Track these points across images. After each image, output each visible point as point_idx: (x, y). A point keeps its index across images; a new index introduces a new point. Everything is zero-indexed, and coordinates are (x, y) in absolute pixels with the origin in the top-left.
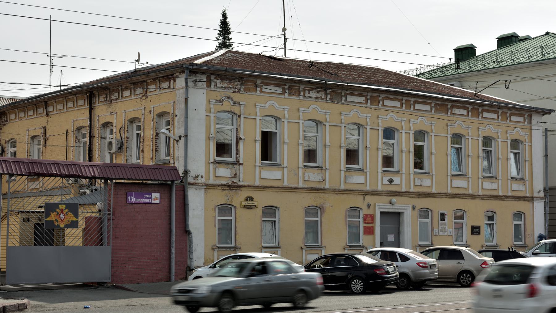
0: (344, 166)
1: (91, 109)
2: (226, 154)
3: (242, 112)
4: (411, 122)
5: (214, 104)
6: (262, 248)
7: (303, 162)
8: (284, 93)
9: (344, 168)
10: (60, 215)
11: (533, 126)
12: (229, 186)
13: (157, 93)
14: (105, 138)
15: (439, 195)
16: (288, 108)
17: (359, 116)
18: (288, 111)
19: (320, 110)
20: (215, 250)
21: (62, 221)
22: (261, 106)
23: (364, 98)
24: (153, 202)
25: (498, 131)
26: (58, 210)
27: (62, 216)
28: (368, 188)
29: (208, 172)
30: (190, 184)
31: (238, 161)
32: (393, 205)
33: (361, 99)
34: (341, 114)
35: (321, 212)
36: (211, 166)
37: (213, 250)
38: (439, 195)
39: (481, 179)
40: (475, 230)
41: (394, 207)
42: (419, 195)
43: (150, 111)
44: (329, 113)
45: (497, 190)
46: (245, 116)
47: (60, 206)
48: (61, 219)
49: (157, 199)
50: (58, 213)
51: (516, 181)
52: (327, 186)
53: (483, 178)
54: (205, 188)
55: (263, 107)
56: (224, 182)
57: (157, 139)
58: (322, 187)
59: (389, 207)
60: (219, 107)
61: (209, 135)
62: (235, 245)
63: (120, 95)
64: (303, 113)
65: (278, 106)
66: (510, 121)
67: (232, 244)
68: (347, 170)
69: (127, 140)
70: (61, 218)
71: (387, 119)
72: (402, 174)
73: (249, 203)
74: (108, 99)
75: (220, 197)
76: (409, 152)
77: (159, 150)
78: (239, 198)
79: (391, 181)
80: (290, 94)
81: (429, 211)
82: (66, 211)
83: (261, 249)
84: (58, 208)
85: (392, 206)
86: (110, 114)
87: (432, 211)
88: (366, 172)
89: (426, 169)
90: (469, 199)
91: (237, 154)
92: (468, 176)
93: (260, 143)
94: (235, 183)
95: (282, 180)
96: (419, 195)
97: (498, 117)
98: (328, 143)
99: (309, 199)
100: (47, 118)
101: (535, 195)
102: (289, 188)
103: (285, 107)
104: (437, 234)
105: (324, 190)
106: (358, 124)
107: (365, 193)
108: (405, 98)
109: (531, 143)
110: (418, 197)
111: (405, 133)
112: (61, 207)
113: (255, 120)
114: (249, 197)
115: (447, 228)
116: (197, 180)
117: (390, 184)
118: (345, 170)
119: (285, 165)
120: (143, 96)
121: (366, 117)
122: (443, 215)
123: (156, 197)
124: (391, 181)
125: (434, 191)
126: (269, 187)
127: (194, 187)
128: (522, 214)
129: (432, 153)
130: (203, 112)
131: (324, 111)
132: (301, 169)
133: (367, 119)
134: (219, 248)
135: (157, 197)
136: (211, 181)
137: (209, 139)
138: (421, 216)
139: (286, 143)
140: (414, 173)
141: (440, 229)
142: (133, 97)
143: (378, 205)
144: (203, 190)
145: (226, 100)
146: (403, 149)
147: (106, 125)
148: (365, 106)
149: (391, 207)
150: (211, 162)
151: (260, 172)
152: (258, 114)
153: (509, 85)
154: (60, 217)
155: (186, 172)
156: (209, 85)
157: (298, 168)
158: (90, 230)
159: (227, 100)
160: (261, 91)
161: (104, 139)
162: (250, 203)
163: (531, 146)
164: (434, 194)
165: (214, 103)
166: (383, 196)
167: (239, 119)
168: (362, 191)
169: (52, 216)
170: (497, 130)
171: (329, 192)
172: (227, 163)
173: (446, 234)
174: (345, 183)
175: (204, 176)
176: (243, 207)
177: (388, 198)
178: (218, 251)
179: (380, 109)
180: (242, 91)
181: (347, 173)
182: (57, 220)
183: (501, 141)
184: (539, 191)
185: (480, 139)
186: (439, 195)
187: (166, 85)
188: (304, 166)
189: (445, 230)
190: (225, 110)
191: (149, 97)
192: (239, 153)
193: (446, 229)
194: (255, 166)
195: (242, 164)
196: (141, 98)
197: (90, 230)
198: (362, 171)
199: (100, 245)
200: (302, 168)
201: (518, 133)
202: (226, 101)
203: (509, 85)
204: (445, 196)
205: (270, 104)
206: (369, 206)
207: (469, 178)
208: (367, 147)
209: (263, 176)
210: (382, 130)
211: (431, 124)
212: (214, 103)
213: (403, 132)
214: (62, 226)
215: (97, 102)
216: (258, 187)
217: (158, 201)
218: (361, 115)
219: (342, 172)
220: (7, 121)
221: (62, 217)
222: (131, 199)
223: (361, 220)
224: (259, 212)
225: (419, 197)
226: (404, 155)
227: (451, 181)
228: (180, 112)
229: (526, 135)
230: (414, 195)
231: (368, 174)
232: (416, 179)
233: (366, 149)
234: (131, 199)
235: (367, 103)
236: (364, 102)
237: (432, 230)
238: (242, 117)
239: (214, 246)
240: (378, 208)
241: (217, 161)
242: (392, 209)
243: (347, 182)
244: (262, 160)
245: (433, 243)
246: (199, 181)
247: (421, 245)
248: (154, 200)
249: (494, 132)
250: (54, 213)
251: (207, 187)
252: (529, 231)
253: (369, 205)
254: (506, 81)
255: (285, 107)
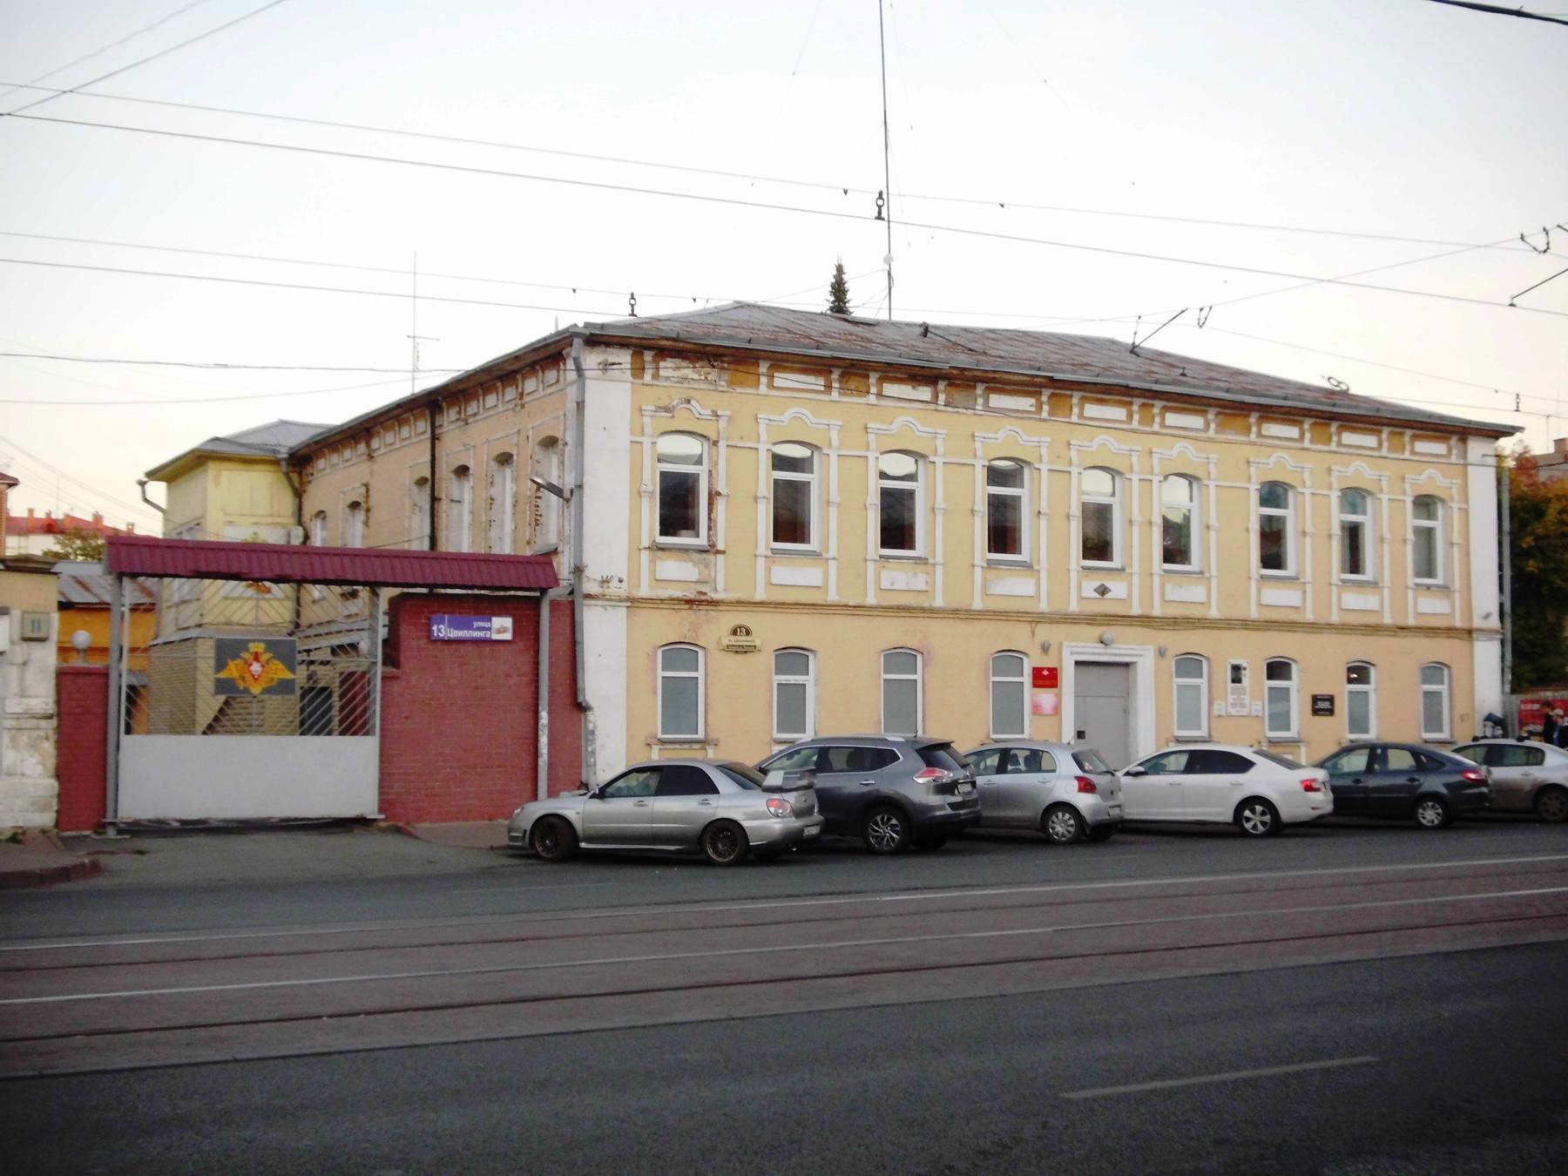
0: (767, 543)
1: (434, 438)
2: (687, 529)
3: (722, 435)
4: (1154, 455)
5: (652, 417)
6: (773, 743)
7: (1162, 561)
8: (829, 387)
9: (766, 550)
10: (251, 665)
11: (590, 379)
12: (690, 602)
13: (538, 396)
14: (459, 502)
15: (1229, 624)
16: (1049, 440)
17: (1021, 442)
18: (839, 431)
19: (920, 428)
20: (653, 746)
21: (256, 680)
22: (770, 420)
23: (1032, 401)
24: (495, 637)
25: (1208, 458)
26: (246, 655)
27: (256, 667)
28: (1043, 606)
29: (634, 569)
30: (589, 596)
31: (713, 545)
32: (1106, 645)
33: (1026, 403)
34: (974, 436)
35: (923, 661)
36: (645, 555)
37: (648, 748)
38: (1227, 624)
39: (1337, 585)
40: (1321, 705)
41: (1108, 651)
42: (1173, 623)
43: (528, 437)
44: (941, 434)
45: (1380, 612)
46: (730, 443)
47: (251, 645)
48: (253, 676)
49: (504, 632)
50: (246, 661)
51: (1428, 592)
52: (939, 603)
53: (1340, 583)
54: (628, 607)
55: (776, 423)
56: (678, 594)
57: (539, 498)
58: (926, 605)
59: (1097, 651)
60: (665, 422)
61: (640, 487)
62: (1210, 735)
63: (481, 405)
64: (876, 434)
65: (1117, 446)
66: (1339, 444)
67: (697, 733)
68: (990, 563)
69: (491, 504)
70: (253, 673)
71: (1093, 449)
72: (1131, 574)
73: (738, 641)
74: (463, 416)
75: (670, 626)
76: (1150, 523)
77: (542, 521)
78: (715, 630)
79: (1103, 591)
80: (844, 390)
81: (1201, 661)
82: (267, 656)
83: (771, 746)
84: (247, 650)
85: (1105, 648)
86: (463, 448)
87: (1208, 659)
88: (1038, 571)
89: (1368, 575)
90: (1304, 632)
91: (710, 528)
92: (1302, 580)
93: (876, 510)
94: (705, 594)
95: (1380, 612)
96: (1173, 623)
97: (1380, 444)
98: (940, 503)
99: (896, 632)
100: (370, 463)
101: (1478, 623)
102: (839, 606)
103: (832, 422)
104: (1223, 713)
105: (931, 612)
106: (1114, 470)
107: (1038, 619)
108: (1138, 402)
109: (1466, 501)
110: (1172, 628)
111: (1140, 480)
112: (253, 647)
113: (755, 451)
114: (740, 628)
115: (1247, 699)
116: (608, 587)
117: (1099, 596)
118: (985, 565)
119: (833, 552)
120: (516, 405)
121: (1037, 444)
122: (1236, 669)
123: (501, 626)
124: (1103, 591)
125: (1214, 613)
126: (809, 605)
127: (600, 603)
128: (697, 652)
129: (1208, 527)
130: (623, 437)
131: (932, 430)
132: (872, 563)
133: (1042, 448)
134: (662, 742)
135: (505, 625)
136: (644, 591)
137: (640, 496)
138: (1180, 672)
139: (834, 503)
140: (1162, 573)
141: (1230, 700)
142: (501, 408)
143: (1068, 647)
144: (625, 610)
145: (682, 406)
146: (1134, 519)
147: (462, 471)
148: (1298, 445)
149: (1102, 651)
150: (645, 548)
151: (1339, 597)
152: (763, 437)
153: (1206, 319)
154: (250, 672)
155: (578, 570)
156: (638, 370)
157: (866, 560)
158: (353, 698)
159: (684, 405)
160: (771, 386)
161: (458, 504)
162: (742, 640)
163: (1465, 512)
164: (1214, 621)
165: (651, 414)
166: (1083, 625)
167: (715, 448)
168: (1027, 613)
169: (230, 669)
170: (1378, 473)
171: (941, 616)
172: (685, 550)
173: (1244, 713)
174: (985, 594)
175: (625, 577)
176: (724, 650)
177: (1096, 631)
178: (660, 749)
179: (1252, 444)
180: (723, 386)
181: (991, 574)
182: (243, 678)
183: (1390, 499)
184: (1487, 616)
185: (1335, 495)
186: (1227, 624)
187: (551, 375)
188: (881, 557)
189: (1243, 705)
190: (681, 429)
191: (526, 405)
192: (716, 526)
193: (1247, 701)
194: (756, 556)
195: (723, 552)
196: (513, 409)
197: (353, 698)
198: (1027, 566)
199: (326, 735)
200: (875, 561)
201: (1432, 479)
202: (681, 408)
203: (1206, 319)
204: (1242, 625)
205: (793, 415)
206: (1045, 649)
207: (1305, 583)
208: (1039, 512)
209: (885, 584)
210: (984, 466)
211: (1206, 460)
212: (651, 414)
213: (1135, 478)
214: (256, 690)
215: (445, 424)
216: (762, 603)
217: (508, 636)
218: (1025, 438)
219: (978, 571)
220: (312, 474)
221: (256, 671)
222: (439, 630)
223: (1027, 679)
224: (767, 660)
225: (1176, 628)
226: (1136, 530)
227: (1259, 591)
228: (570, 438)
229: (1454, 486)
230: (1161, 622)
231: (1044, 575)
232: (1168, 587)
233: (1039, 518)
234: (439, 630)
235: (937, 400)
236: (1033, 409)
237: (1211, 704)
238: (722, 444)
239: (651, 738)
240: (1069, 653)
241: (659, 546)
242: (1106, 654)
243: (991, 592)
244: (776, 539)
245: (1212, 733)
246: (614, 589)
247: (1273, 740)
248: (499, 632)
249: (700, 417)
250: (236, 662)
251: (634, 603)
252: (1461, 708)
253: (1046, 645)
254: (1201, 310)
255: (832, 422)
